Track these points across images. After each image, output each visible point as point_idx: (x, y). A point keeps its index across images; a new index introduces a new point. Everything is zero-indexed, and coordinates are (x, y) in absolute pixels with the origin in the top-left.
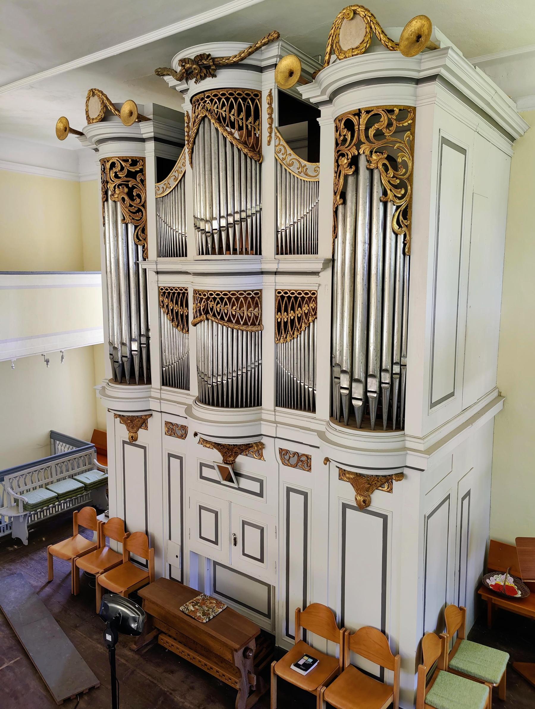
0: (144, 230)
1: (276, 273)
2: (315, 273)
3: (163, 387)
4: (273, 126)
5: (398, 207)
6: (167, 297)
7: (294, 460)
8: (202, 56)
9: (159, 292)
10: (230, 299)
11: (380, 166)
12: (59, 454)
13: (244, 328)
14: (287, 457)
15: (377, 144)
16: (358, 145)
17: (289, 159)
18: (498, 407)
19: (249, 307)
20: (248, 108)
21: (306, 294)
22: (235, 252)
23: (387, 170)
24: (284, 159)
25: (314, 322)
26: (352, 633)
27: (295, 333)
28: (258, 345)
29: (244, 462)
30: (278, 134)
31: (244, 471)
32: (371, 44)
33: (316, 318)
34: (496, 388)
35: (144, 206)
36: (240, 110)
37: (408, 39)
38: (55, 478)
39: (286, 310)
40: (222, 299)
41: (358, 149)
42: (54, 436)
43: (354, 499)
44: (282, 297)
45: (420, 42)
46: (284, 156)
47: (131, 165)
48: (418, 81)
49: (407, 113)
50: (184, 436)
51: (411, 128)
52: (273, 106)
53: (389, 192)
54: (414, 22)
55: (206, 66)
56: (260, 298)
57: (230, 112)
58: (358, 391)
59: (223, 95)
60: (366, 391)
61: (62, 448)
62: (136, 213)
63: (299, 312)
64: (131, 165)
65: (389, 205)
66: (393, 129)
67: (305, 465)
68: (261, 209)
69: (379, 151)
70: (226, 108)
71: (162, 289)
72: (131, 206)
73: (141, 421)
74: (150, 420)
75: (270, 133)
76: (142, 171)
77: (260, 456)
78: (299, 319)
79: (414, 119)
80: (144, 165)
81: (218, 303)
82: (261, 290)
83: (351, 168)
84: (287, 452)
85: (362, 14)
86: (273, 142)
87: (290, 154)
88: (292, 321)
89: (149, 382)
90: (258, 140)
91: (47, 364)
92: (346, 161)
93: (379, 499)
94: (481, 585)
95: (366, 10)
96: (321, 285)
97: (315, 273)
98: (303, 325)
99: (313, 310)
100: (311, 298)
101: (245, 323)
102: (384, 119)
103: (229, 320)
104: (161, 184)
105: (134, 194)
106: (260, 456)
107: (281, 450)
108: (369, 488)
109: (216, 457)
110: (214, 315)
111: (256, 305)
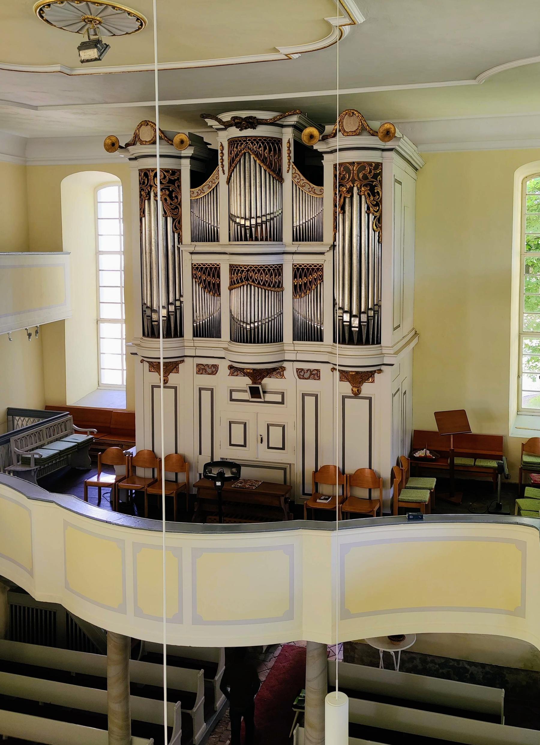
0: (180, 222)
1: (293, 253)
2: (323, 253)
3: (195, 338)
4: (291, 161)
5: (375, 217)
6: (199, 271)
7: (307, 375)
8: (250, 117)
9: (192, 268)
10: (264, 270)
11: (366, 193)
12: (18, 429)
13: (273, 289)
14: (302, 374)
15: (366, 182)
16: (353, 181)
17: (302, 182)
18: (415, 341)
19: (275, 276)
20: (270, 148)
21: (315, 266)
22: (257, 239)
23: (369, 196)
24: (298, 182)
25: (320, 284)
26: (351, 476)
27: (308, 291)
28: (281, 301)
29: (269, 383)
30: (294, 166)
31: (269, 388)
32: (363, 129)
33: (323, 281)
34: (413, 329)
35: (180, 204)
36: (270, 150)
37: (382, 132)
38: (46, 441)
39: (301, 277)
40: (259, 270)
41: (353, 183)
42: (12, 412)
43: (351, 392)
44: (298, 269)
45: (388, 135)
46: (299, 181)
47: (171, 175)
48: (383, 150)
49: (378, 165)
50: (215, 372)
51: (380, 174)
52: (291, 149)
53: (371, 208)
54: (386, 125)
55: (252, 123)
56: (282, 269)
57: (264, 151)
58: (355, 322)
59: (260, 140)
60: (360, 322)
61: (21, 422)
62: (173, 209)
63: (310, 278)
64: (171, 175)
65: (371, 215)
66: (372, 174)
67: (316, 377)
68: (282, 212)
69: (365, 185)
70: (262, 148)
71: (195, 265)
72: (171, 204)
73: (174, 365)
74: (180, 365)
75: (289, 165)
76: (179, 179)
77: (282, 376)
78: (310, 282)
79: (382, 169)
80: (180, 175)
81: (256, 273)
82: (282, 265)
83: (349, 193)
84: (302, 370)
85: (357, 115)
86: (290, 171)
87: (303, 180)
88: (300, 286)
89: (182, 336)
90: (280, 170)
91: (29, 338)
92: (345, 189)
93: (366, 388)
94: (411, 456)
95: (359, 113)
96: (326, 261)
97: (323, 253)
98: (313, 286)
99: (320, 276)
100: (319, 269)
101: (274, 286)
102: (368, 169)
103: (264, 285)
104: (196, 190)
105: (174, 196)
106: (282, 376)
107: (298, 370)
108: (360, 382)
109: (245, 382)
110: (253, 281)
111: (280, 275)
